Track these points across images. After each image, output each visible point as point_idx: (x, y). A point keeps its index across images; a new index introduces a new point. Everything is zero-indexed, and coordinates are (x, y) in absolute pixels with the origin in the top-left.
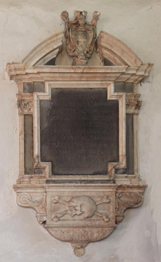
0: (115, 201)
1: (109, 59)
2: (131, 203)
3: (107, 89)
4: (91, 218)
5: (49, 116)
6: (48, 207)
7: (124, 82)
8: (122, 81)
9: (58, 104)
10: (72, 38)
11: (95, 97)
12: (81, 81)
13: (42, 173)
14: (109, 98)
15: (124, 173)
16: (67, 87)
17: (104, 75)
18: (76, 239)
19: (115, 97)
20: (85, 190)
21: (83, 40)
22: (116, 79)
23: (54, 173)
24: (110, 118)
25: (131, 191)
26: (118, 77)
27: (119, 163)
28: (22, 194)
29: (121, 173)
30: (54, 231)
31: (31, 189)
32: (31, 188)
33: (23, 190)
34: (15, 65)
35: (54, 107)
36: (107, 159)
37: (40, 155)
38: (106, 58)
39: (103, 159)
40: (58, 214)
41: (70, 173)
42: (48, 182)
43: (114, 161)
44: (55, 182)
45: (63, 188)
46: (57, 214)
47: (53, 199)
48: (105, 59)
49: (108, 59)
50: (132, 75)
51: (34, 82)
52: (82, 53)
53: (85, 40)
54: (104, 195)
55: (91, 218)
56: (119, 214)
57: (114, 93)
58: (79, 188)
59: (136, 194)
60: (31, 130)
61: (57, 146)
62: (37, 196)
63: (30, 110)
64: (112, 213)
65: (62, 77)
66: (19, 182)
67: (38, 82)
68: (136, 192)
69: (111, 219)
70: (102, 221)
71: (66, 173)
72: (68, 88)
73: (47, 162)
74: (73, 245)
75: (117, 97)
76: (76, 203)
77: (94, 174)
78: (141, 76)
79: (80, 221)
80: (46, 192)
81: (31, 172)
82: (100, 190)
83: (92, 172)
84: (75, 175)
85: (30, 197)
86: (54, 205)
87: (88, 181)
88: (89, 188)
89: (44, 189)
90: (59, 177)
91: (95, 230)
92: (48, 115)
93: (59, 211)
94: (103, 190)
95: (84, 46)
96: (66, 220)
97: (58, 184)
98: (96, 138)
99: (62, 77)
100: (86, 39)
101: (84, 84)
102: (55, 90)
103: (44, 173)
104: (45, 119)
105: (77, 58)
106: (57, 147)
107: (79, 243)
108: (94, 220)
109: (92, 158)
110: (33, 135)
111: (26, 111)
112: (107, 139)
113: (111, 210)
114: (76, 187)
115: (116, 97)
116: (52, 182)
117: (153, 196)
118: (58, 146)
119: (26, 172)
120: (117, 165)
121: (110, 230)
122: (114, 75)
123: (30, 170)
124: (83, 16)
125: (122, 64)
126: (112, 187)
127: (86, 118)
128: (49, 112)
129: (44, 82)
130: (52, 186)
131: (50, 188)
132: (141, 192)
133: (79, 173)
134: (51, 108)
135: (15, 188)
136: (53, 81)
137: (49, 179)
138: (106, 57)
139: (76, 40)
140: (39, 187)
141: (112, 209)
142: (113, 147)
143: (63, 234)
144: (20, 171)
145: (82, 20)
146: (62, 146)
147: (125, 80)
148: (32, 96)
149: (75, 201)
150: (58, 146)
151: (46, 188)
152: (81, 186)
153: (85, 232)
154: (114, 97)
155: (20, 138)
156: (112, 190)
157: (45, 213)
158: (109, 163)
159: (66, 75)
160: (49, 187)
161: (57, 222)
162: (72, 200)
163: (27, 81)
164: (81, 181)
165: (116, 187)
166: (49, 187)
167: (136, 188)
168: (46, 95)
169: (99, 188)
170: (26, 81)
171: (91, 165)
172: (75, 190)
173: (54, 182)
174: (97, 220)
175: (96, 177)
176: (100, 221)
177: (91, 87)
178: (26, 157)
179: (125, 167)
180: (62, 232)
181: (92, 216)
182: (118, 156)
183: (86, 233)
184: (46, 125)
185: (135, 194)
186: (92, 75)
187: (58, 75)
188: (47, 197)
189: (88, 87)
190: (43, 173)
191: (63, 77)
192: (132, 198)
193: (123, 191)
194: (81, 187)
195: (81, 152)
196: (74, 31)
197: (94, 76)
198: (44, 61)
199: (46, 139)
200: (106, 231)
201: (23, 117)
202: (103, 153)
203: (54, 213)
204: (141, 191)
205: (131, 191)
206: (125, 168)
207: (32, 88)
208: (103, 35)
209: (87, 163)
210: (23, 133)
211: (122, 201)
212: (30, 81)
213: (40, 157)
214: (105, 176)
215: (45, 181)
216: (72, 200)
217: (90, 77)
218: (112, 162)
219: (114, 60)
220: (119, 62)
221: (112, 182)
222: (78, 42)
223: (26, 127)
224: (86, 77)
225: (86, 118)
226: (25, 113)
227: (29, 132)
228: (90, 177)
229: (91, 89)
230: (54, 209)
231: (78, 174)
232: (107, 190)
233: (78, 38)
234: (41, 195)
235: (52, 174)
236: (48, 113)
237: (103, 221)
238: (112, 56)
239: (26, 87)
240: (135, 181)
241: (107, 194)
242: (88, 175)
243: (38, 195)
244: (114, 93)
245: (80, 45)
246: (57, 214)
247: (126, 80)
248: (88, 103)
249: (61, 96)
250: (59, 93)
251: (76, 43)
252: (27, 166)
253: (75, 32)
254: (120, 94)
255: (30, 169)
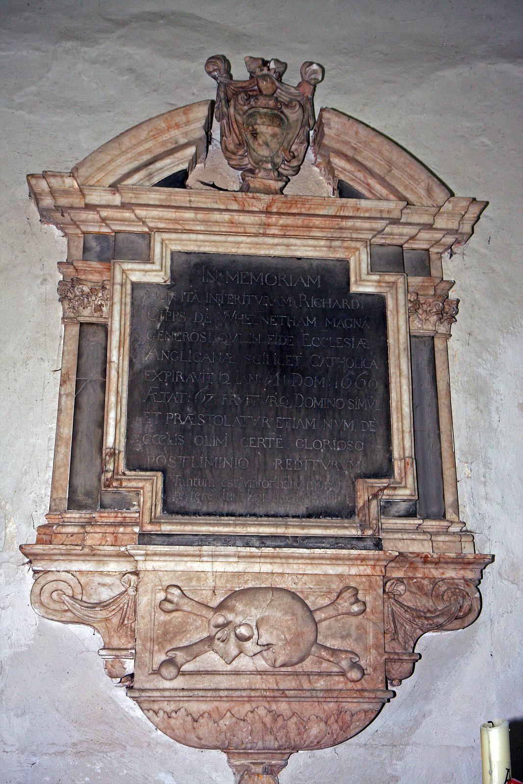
0: (381, 608)
1: (351, 183)
2: (438, 616)
3: (348, 262)
4: (297, 666)
5: (160, 329)
6: (142, 624)
7: (401, 246)
8: (395, 242)
9: (191, 296)
10: (236, 121)
11: (311, 283)
12: (265, 235)
13: (128, 506)
14: (354, 289)
15: (411, 514)
16: (221, 250)
17: (336, 222)
18: (243, 743)
19: (372, 286)
20: (277, 569)
21: (270, 128)
22: (374, 236)
23: (171, 510)
24: (361, 345)
25: (436, 573)
26: (380, 232)
27: (392, 480)
28: (50, 577)
29: (402, 513)
30: (161, 713)
31: (84, 561)
32: (81, 558)
33: (56, 563)
34: (53, 181)
35: (176, 305)
36: (352, 467)
37: (122, 449)
38: (343, 181)
39: (341, 468)
40: (178, 653)
41: (226, 508)
42: (146, 539)
43: (376, 475)
44: (172, 539)
45: (197, 559)
46: (173, 649)
47: (161, 596)
48: (340, 182)
49: (348, 181)
50: (420, 227)
51: (117, 232)
52: (267, 162)
53: (277, 130)
54: (341, 586)
55: (298, 668)
56: (398, 654)
57: (368, 274)
58: (253, 560)
59: (451, 582)
60: (99, 369)
61: (183, 420)
62: (104, 585)
63: (101, 310)
64: (373, 651)
65: (203, 222)
66: (46, 534)
67: (130, 233)
68: (453, 579)
69: (369, 670)
70: (336, 678)
71: (212, 508)
72: (225, 255)
73: (146, 470)
74: (237, 763)
75: (381, 286)
76: (245, 616)
77: (309, 516)
78: (449, 232)
79: (259, 677)
80: (136, 573)
81: (90, 501)
82: (331, 570)
83: (302, 510)
84: (246, 516)
85: (78, 590)
86: (163, 617)
87: (287, 537)
88: (291, 561)
89: (130, 561)
90: (185, 524)
91: (310, 710)
92: (158, 328)
93: (181, 640)
94: (339, 570)
95: (274, 145)
96: (207, 673)
97: (177, 548)
98: (315, 401)
99: (203, 222)
100: (279, 126)
101: (277, 245)
102: (184, 257)
103: (136, 507)
104: (145, 336)
105: (254, 174)
106: (183, 423)
107: (255, 756)
108: (308, 674)
109: (304, 462)
110: (103, 386)
111: (87, 315)
112: (351, 406)
113: (371, 640)
114: (244, 557)
115: (375, 284)
116: (159, 538)
117: (497, 591)
118: (188, 421)
119: (73, 503)
120: (385, 488)
121: (366, 712)
122: (367, 225)
123: (88, 494)
124: (269, 69)
125: (391, 197)
126: (370, 559)
127: (283, 341)
128: (162, 318)
129: (150, 235)
130: (155, 554)
131: (148, 558)
132: (471, 580)
133: (257, 510)
134: (167, 308)
135: (60, 300)
136: (175, 231)
137: (149, 528)
138: (342, 177)
139: (250, 128)
140: (110, 556)
141: (371, 634)
142: (371, 432)
143: (195, 724)
144: (55, 496)
145: (266, 81)
146: (201, 422)
147: (402, 242)
148: (109, 269)
149: (240, 607)
150: (188, 421)
151: (137, 558)
152: (260, 557)
153: (276, 716)
154: (369, 286)
155: (62, 393)
156: (369, 571)
157: (130, 646)
158: (360, 481)
159: (217, 216)
160: (147, 555)
161: (171, 680)
162: (231, 603)
163: (96, 230)
164: (263, 540)
165: (382, 560)
166: (147, 555)
167: (453, 566)
168: (155, 274)
169: (324, 562)
170: (91, 229)
171: (299, 484)
172: (240, 567)
173: (169, 539)
174: (320, 674)
175: (315, 527)
176: (329, 678)
177: (299, 254)
178: (77, 451)
179: (411, 495)
180: (189, 718)
181: (302, 660)
182: (390, 460)
183: (280, 722)
184: (148, 357)
185: (452, 584)
186: (299, 221)
187: (190, 215)
188: (141, 590)
189: (290, 254)
190: (134, 505)
191: (207, 222)
192: (440, 597)
193: (411, 575)
194: (262, 560)
195: (267, 442)
196: (245, 105)
197: (301, 217)
198: (150, 176)
199: (149, 399)
200: (352, 715)
201: (76, 329)
202: (338, 449)
203: (164, 648)
204: (470, 575)
205: (436, 573)
206: (413, 498)
207: (110, 249)
208: (329, 119)
209: (287, 479)
210: (74, 377)
211: (408, 607)
212: (105, 230)
213: (122, 455)
214: (346, 522)
215: (136, 533)
216: (231, 603)
217: (292, 226)
218: (369, 477)
219: (368, 187)
220: (384, 192)
221: (369, 543)
222: (255, 135)
223: (83, 360)
224: (281, 226)
225: (283, 341)
226: (82, 319)
227: (94, 374)
228: (294, 526)
229: (299, 259)
230: (165, 633)
231: (253, 512)
232: (354, 571)
233: (256, 124)
234: (118, 582)
235: (164, 509)
236: (159, 321)
237: (342, 679)
238: (360, 175)
239: (93, 244)
240: (451, 541)
241: (353, 584)
242: (287, 516)
243: (107, 580)
244: (368, 274)
245: (261, 142)
246: (173, 649)
247: (407, 242)
248: (290, 299)
249: (200, 277)
250: (197, 266)
251: (249, 136)
252: (79, 481)
253: (246, 108)
254: (390, 278)
255: (84, 493)
